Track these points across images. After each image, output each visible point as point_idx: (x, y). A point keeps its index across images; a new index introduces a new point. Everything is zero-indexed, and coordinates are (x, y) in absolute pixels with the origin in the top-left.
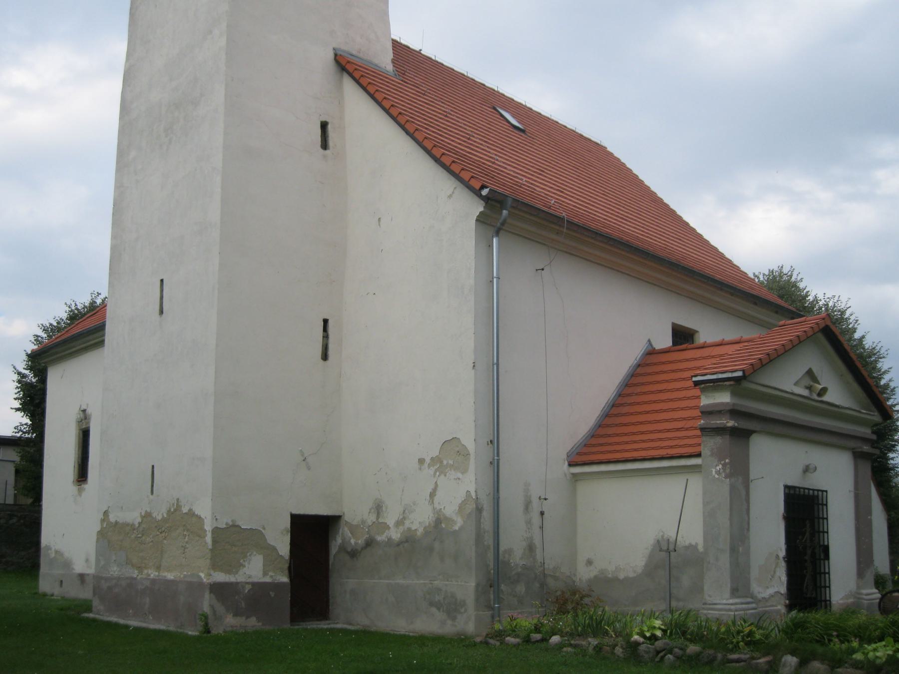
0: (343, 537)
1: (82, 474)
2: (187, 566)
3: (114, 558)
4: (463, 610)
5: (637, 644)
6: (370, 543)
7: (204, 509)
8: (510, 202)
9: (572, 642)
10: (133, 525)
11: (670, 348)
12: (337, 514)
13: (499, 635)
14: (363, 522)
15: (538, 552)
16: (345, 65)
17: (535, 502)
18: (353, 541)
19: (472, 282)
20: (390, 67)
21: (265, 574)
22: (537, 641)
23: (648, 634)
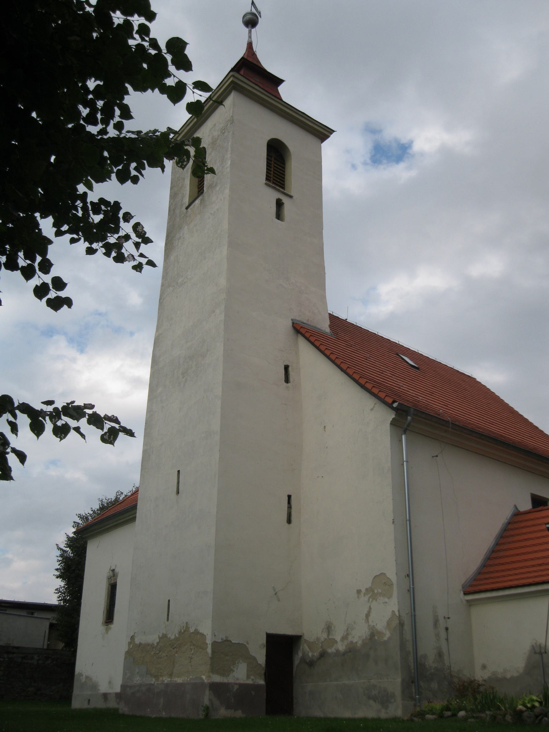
0: (304, 651)
1: (109, 618)
2: (193, 671)
3: (137, 670)
4: (393, 700)
5: (521, 712)
6: (323, 655)
7: (206, 629)
8: (412, 410)
9: (474, 715)
10: (153, 644)
11: (531, 510)
12: (299, 634)
13: (421, 714)
14: (318, 639)
15: (446, 657)
16: (300, 330)
17: (441, 620)
18: (310, 654)
19: (389, 465)
20: (328, 330)
21: (248, 677)
22: (449, 717)
23: (529, 705)
